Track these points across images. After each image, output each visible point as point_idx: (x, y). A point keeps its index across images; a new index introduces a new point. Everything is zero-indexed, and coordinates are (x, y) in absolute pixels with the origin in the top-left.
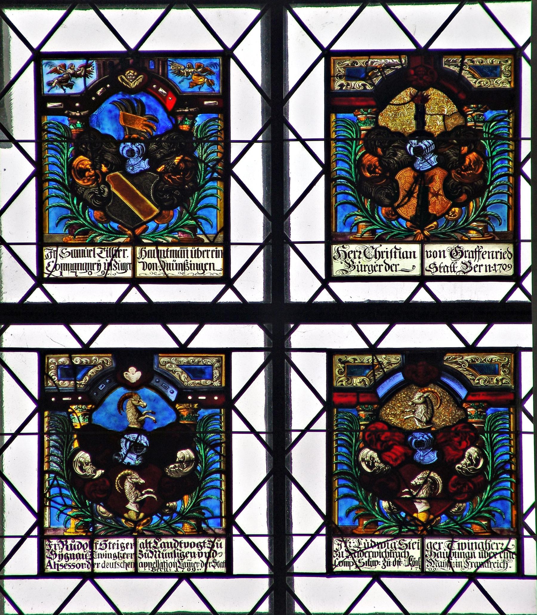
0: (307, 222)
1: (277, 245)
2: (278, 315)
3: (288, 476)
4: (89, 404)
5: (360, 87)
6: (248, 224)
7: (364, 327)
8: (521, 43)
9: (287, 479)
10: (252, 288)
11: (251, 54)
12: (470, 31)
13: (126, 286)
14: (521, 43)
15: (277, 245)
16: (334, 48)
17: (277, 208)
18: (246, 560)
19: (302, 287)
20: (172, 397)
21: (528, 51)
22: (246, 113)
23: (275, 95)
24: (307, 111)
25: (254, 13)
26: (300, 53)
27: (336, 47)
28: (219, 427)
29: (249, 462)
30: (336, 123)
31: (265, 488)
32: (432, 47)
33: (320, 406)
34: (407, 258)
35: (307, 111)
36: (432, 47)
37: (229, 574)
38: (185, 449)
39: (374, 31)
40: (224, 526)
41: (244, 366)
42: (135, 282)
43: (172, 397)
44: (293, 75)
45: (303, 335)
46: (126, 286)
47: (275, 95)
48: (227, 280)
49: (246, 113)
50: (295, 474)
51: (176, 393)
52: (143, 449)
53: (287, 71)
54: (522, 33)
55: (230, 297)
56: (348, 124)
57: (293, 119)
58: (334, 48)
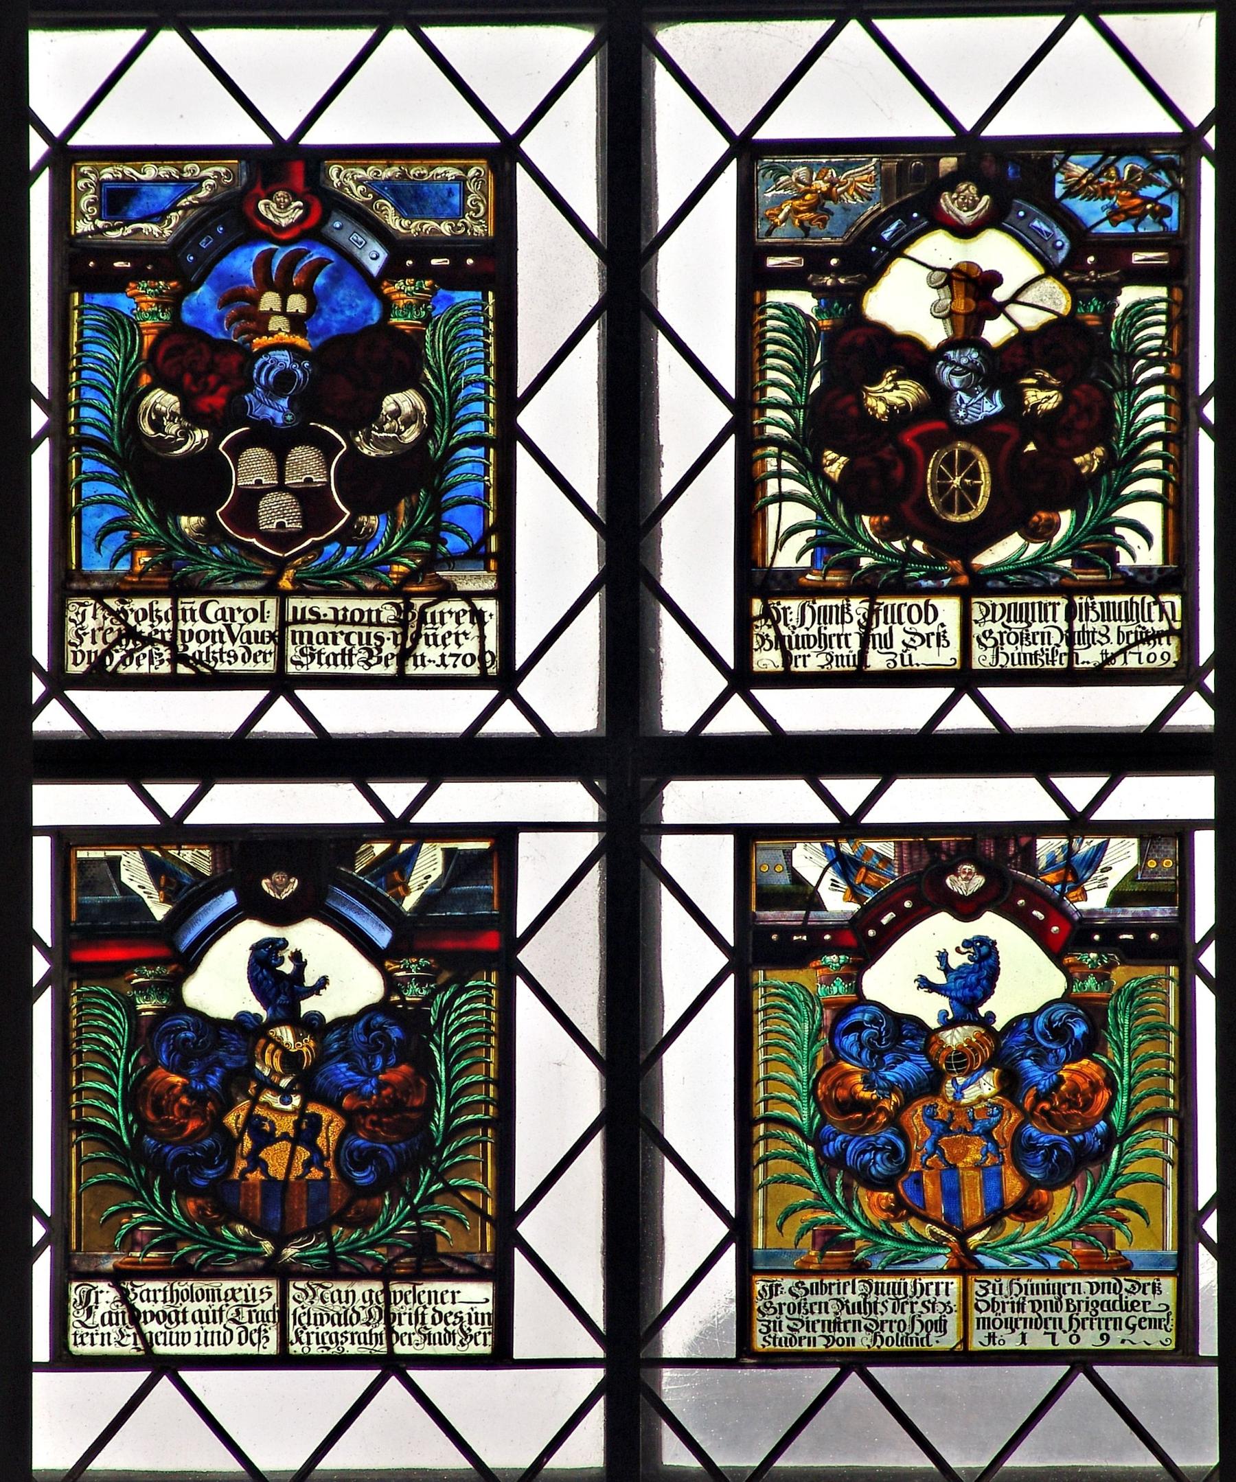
0: (695, 555)
1: (628, 590)
2: (628, 760)
3: (647, 584)
4: (171, 281)
5: (820, 227)
6: (556, 551)
7: (833, 786)
8: (1196, 120)
9: (646, 321)
10: (567, 695)
11: (569, 149)
12: (1081, 89)
13: (260, 695)
14: (1196, 120)
15: (628, 590)
16: (762, 134)
17: (628, 514)
18: (540, 1323)
19: (685, 692)
20: (374, 268)
21: (1210, 138)
22: (557, 278)
23: (627, 239)
24: (696, 281)
25: (578, 39)
26: (682, 147)
27: (766, 133)
28: (481, 333)
29: (556, 1091)
30: (765, 1039)
31: (594, 333)
32: (988, 132)
33: (723, 1230)
34: (931, 629)
35: (696, 281)
36: (988, 132)
37: (501, 1356)
38: (401, 389)
39: (855, 91)
40: (491, 414)
41: (541, 868)
42: (280, 685)
43: (374, 268)
44: (668, 197)
45: (683, 799)
46: (260, 695)
47: (627, 239)
48: (505, 678)
49: (557, 278)
50: (666, 308)
51: (383, 255)
52: (294, 581)
53: (652, 130)
54: (1199, 101)
55: (508, 722)
56: (798, 334)
57: (668, 305)
58: (762, 134)
